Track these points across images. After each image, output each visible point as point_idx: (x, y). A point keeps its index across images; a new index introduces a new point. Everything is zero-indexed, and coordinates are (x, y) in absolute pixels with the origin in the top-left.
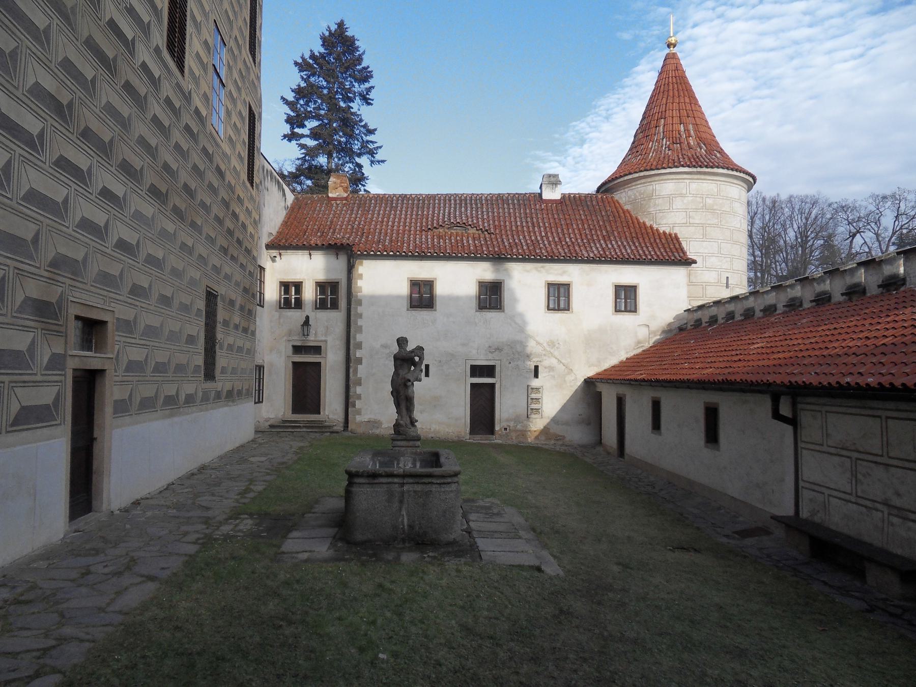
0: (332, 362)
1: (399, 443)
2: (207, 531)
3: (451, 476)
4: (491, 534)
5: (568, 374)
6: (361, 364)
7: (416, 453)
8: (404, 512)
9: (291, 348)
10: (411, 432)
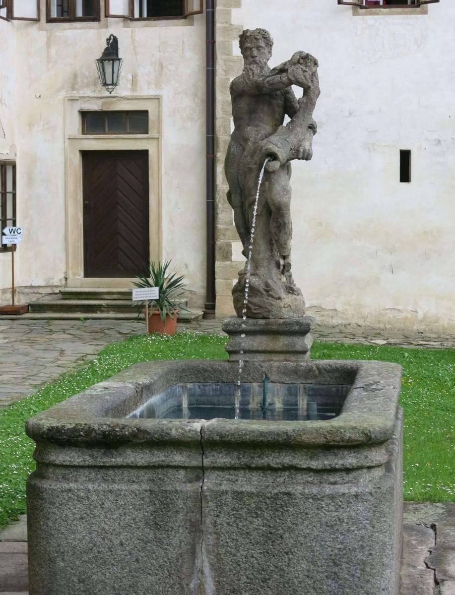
3: (354, 446)
7: (295, 372)
8: (204, 561)
9: (77, 120)
10: (285, 309)
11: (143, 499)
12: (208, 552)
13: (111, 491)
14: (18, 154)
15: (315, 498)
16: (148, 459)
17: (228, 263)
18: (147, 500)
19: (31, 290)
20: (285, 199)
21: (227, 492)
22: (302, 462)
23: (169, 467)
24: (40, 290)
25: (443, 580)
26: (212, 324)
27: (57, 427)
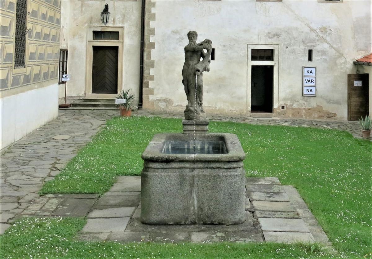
0: (128, 46)
1: (189, 128)
2: (17, 211)
3: (236, 161)
4: (272, 214)
5: (339, 57)
6: (154, 48)
7: (204, 137)
8: (194, 195)
11: (177, 177)
12: (195, 192)
13: (168, 175)
14: (68, 47)
15: (226, 176)
16: (179, 166)
17: (147, 89)
18: (178, 178)
19: (71, 98)
20: (202, 84)
21: (201, 175)
22: (222, 165)
23: (184, 168)
24: (75, 98)
25: (252, 201)
26: (142, 111)
27: (153, 157)
